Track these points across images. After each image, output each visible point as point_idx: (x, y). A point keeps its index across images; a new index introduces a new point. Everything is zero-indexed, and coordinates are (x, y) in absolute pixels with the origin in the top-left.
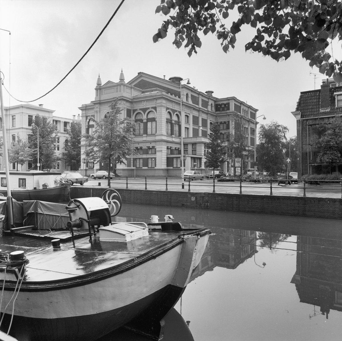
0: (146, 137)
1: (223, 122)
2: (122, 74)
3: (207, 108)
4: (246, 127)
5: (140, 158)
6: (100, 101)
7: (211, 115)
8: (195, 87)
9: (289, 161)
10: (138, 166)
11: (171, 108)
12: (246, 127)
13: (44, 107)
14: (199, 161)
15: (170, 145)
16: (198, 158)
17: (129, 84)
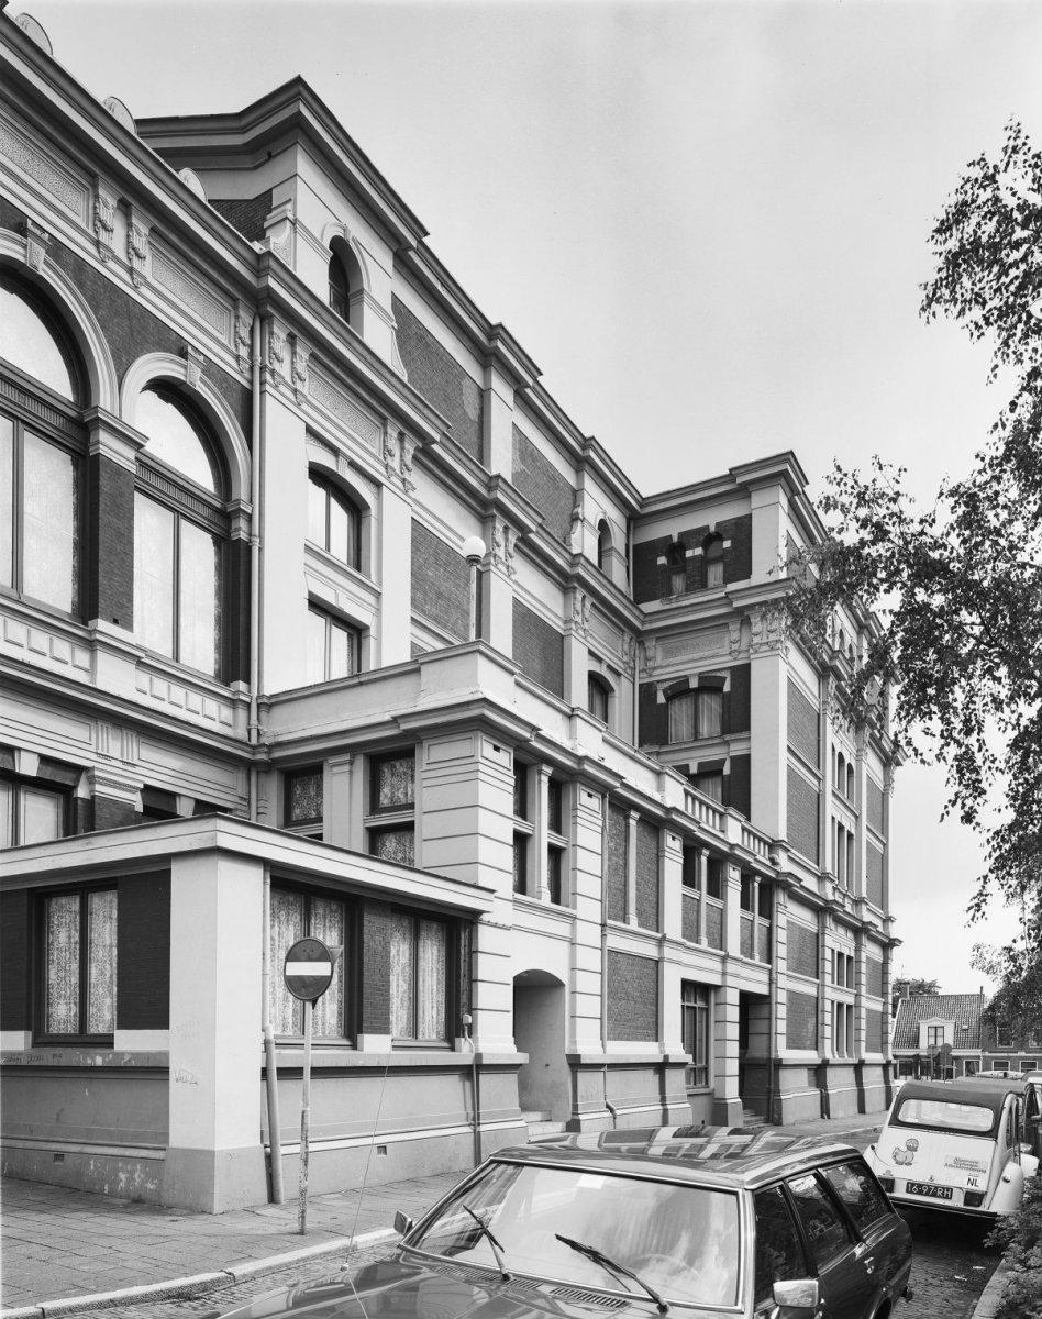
1: (694, 684)
10: (62, 1013)
14: (432, 955)
16: (417, 914)
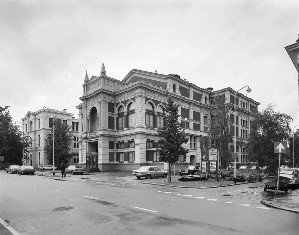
0: (127, 130)
2: (103, 68)
3: (200, 101)
4: (243, 120)
5: (122, 153)
6: (85, 96)
7: (205, 108)
8: (186, 80)
9: (282, 149)
10: (121, 160)
11: (154, 99)
12: (243, 120)
13: (67, 112)
15: (151, 138)
17: (124, 82)
